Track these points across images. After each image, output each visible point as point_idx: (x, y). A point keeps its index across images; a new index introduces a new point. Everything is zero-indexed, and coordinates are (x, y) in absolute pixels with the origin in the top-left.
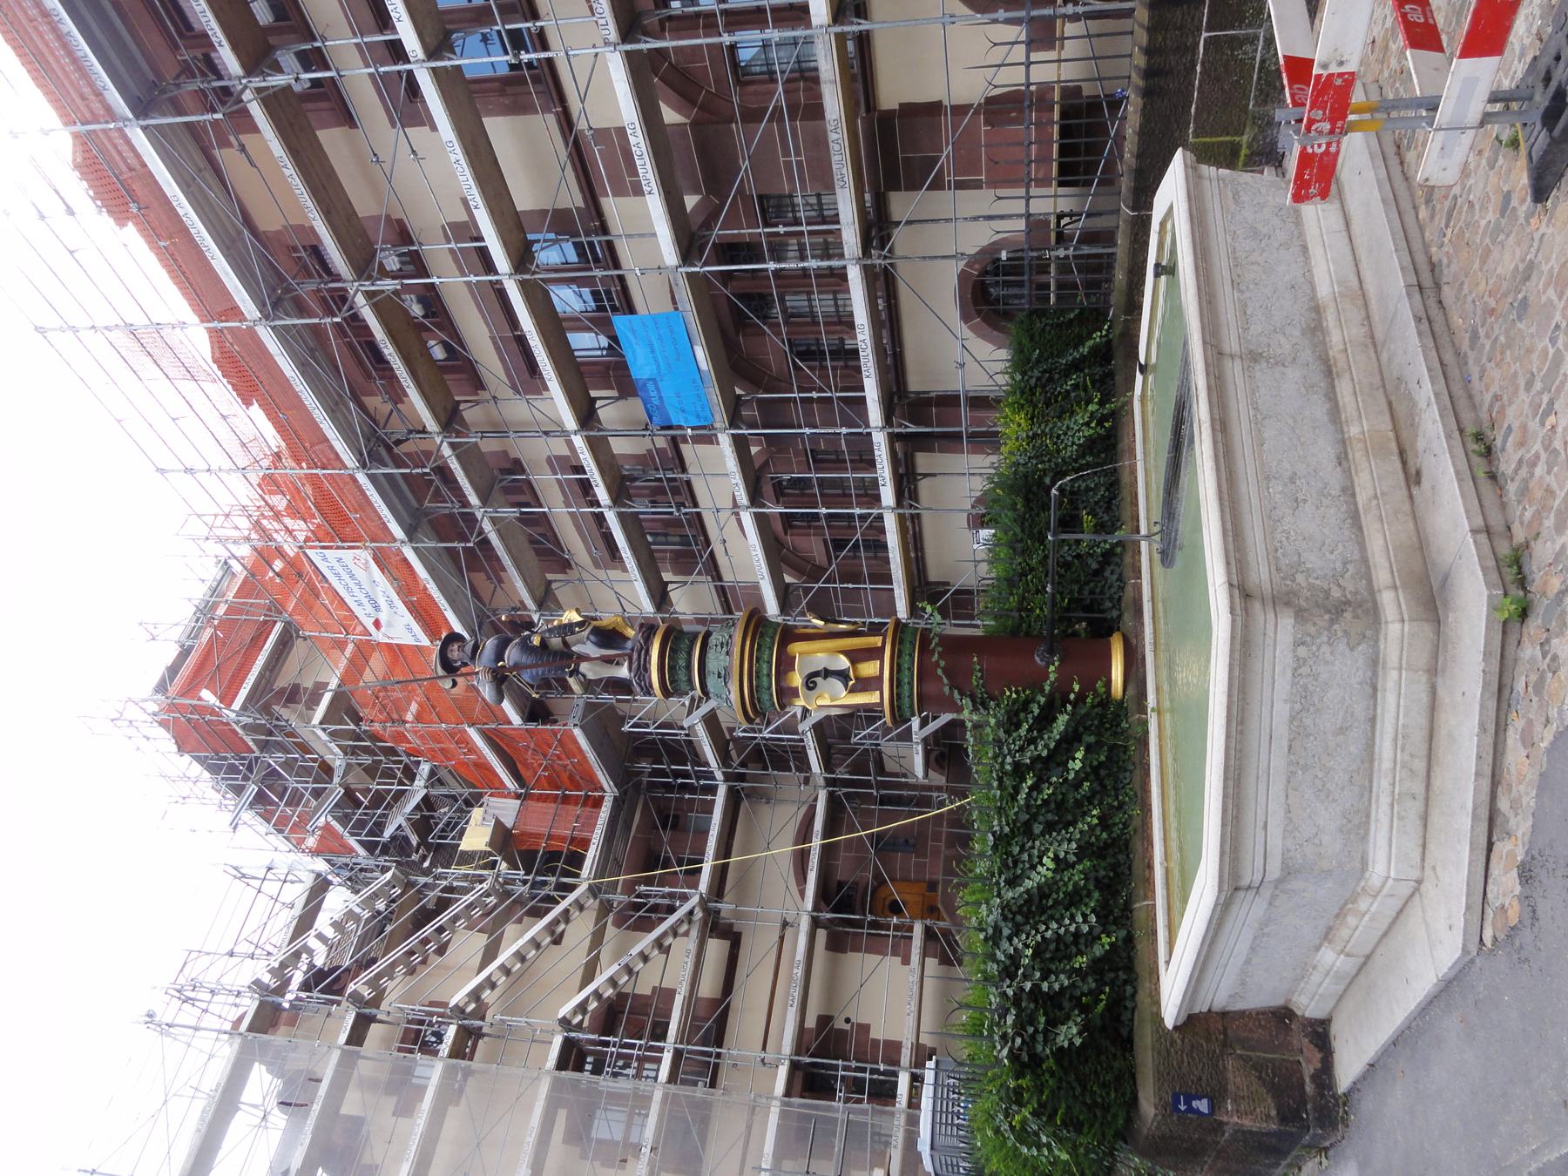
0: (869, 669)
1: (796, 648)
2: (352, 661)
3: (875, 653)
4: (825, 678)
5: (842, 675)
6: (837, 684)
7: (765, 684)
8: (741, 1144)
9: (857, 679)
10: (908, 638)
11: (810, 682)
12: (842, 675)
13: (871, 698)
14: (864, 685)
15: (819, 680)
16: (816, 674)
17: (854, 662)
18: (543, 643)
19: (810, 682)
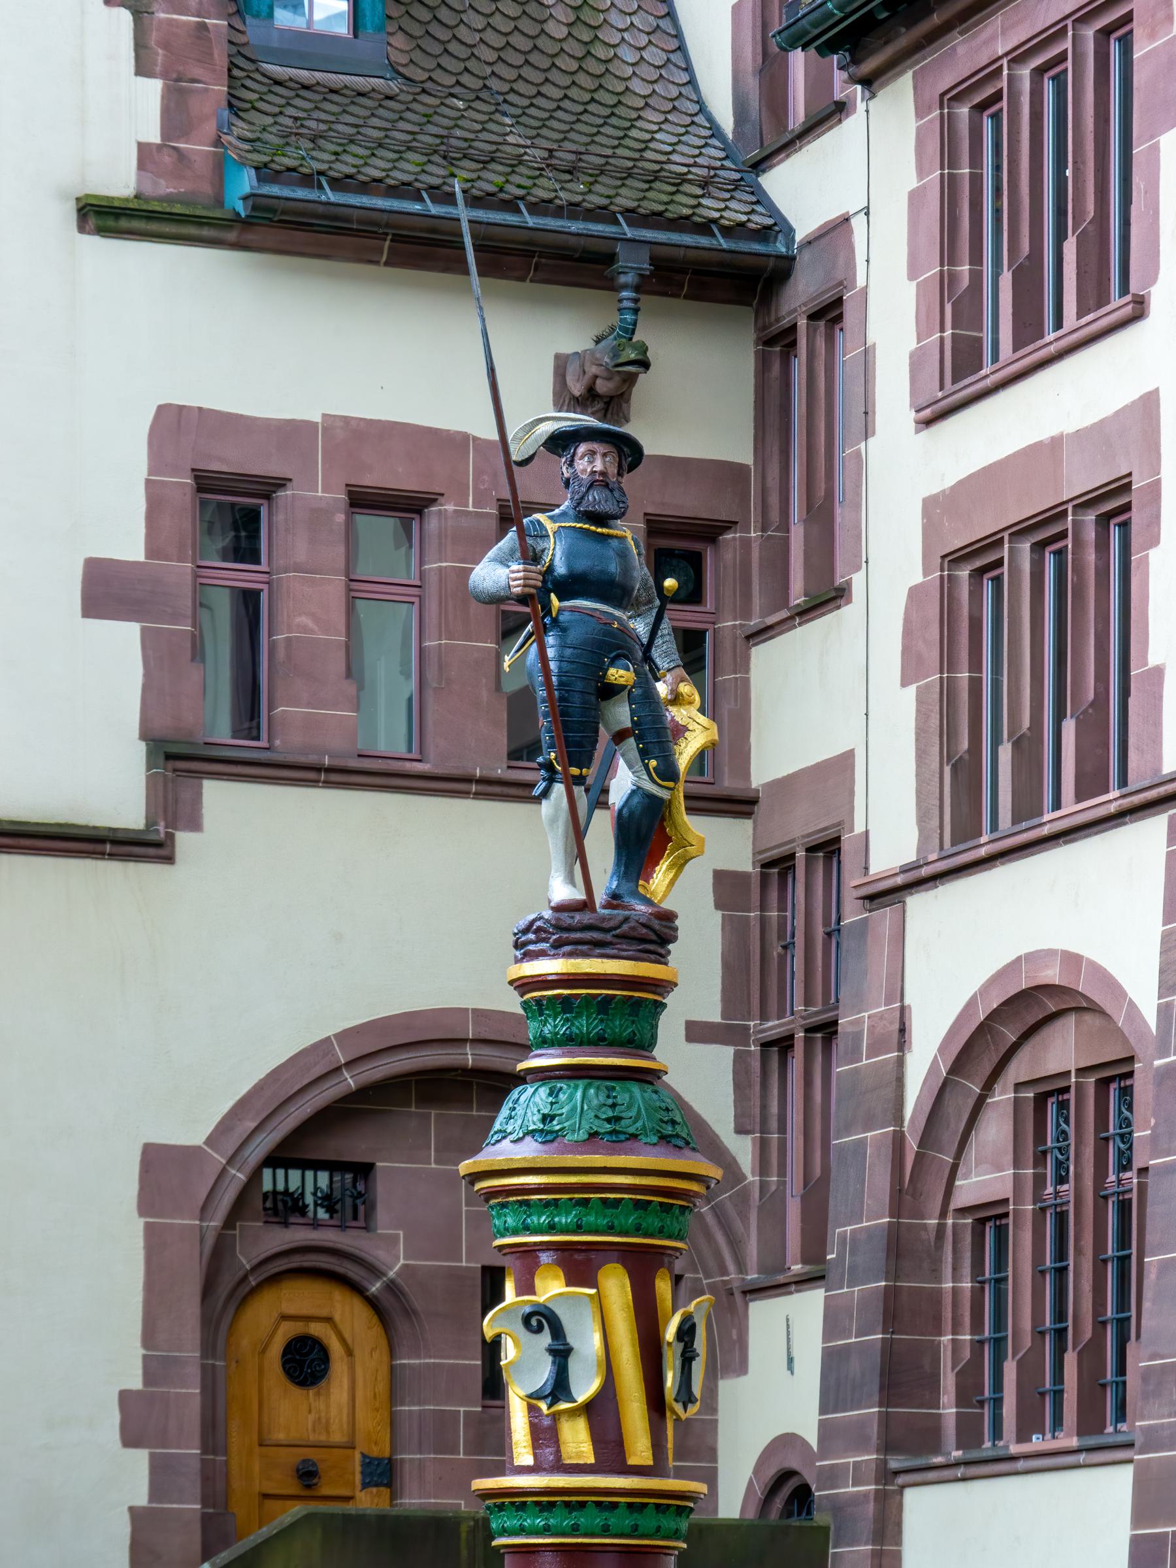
0: (577, 1441)
1: (616, 1285)
2: (658, 613)
3: (610, 1454)
4: (552, 1351)
5: (560, 1388)
6: (543, 1374)
7: (534, 1220)
8: (349, 1341)
9: (555, 1417)
10: (619, 1026)
11: (541, 1319)
12: (560, 1388)
13: (523, 1455)
14: (544, 1435)
15: (545, 1339)
16: (558, 1331)
17: (590, 1409)
18: (610, 691)
19: (541, 1319)
